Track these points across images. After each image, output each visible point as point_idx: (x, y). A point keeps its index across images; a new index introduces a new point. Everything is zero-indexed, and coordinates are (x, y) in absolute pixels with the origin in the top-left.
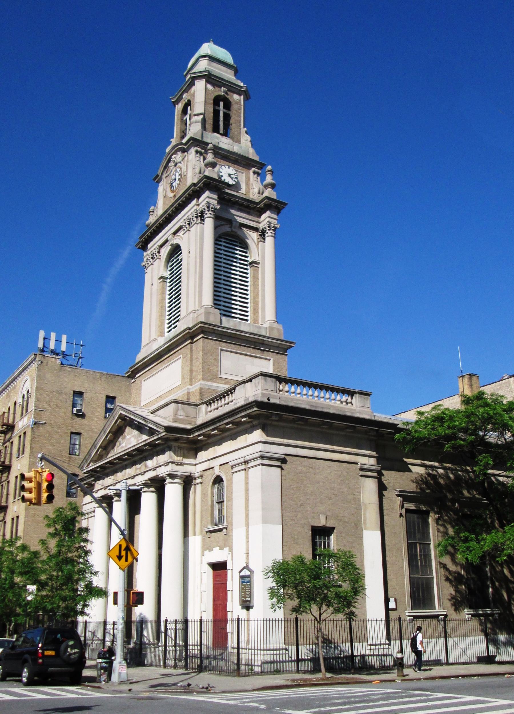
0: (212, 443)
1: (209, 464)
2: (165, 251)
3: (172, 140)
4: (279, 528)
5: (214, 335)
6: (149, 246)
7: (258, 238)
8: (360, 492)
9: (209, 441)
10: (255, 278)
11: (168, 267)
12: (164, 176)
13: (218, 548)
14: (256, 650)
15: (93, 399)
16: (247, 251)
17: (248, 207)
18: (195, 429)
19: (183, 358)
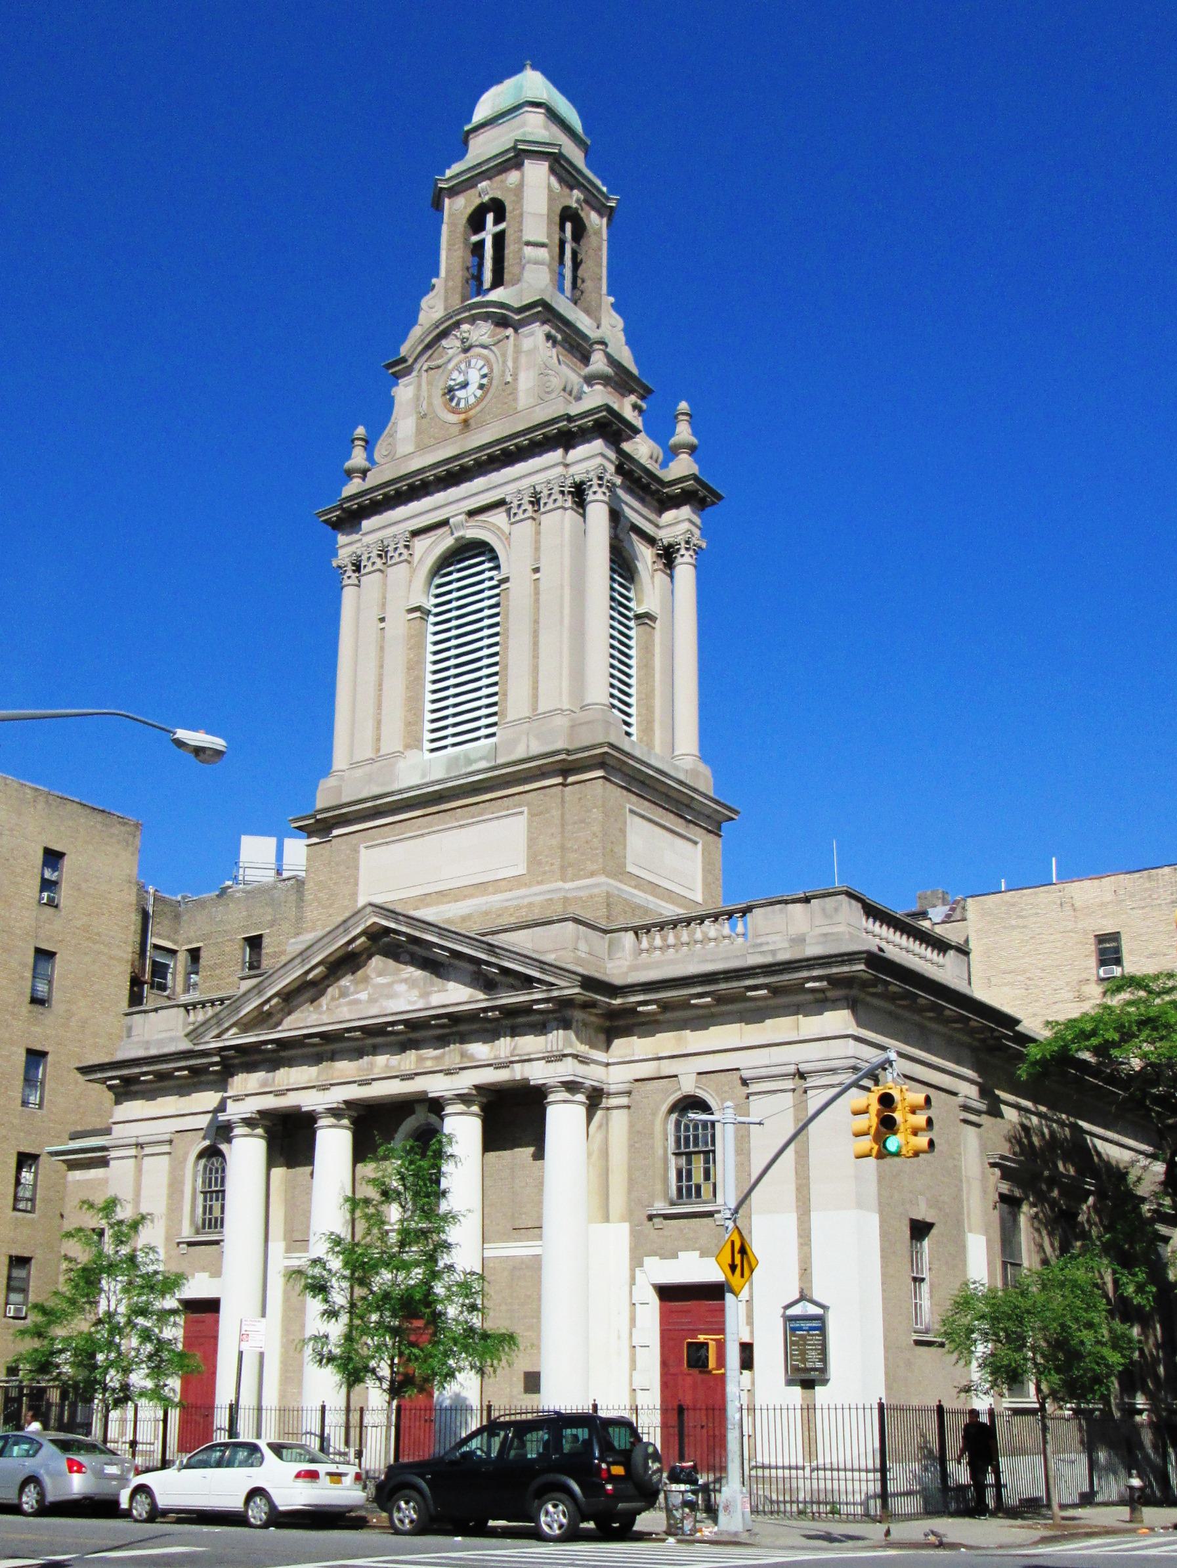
0: (669, 1021)
1: (659, 1068)
2: (428, 550)
3: (434, 281)
4: (874, 1219)
5: (620, 775)
6: (366, 524)
7: (654, 562)
8: (960, 1154)
9: (660, 1017)
10: (647, 649)
11: (433, 587)
12: (422, 364)
13: (697, 1253)
14: (856, 1470)
15: (15, 852)
16: (632, 587)
17: (645, 488)
18: (639, 988)
19: (532, 815)
